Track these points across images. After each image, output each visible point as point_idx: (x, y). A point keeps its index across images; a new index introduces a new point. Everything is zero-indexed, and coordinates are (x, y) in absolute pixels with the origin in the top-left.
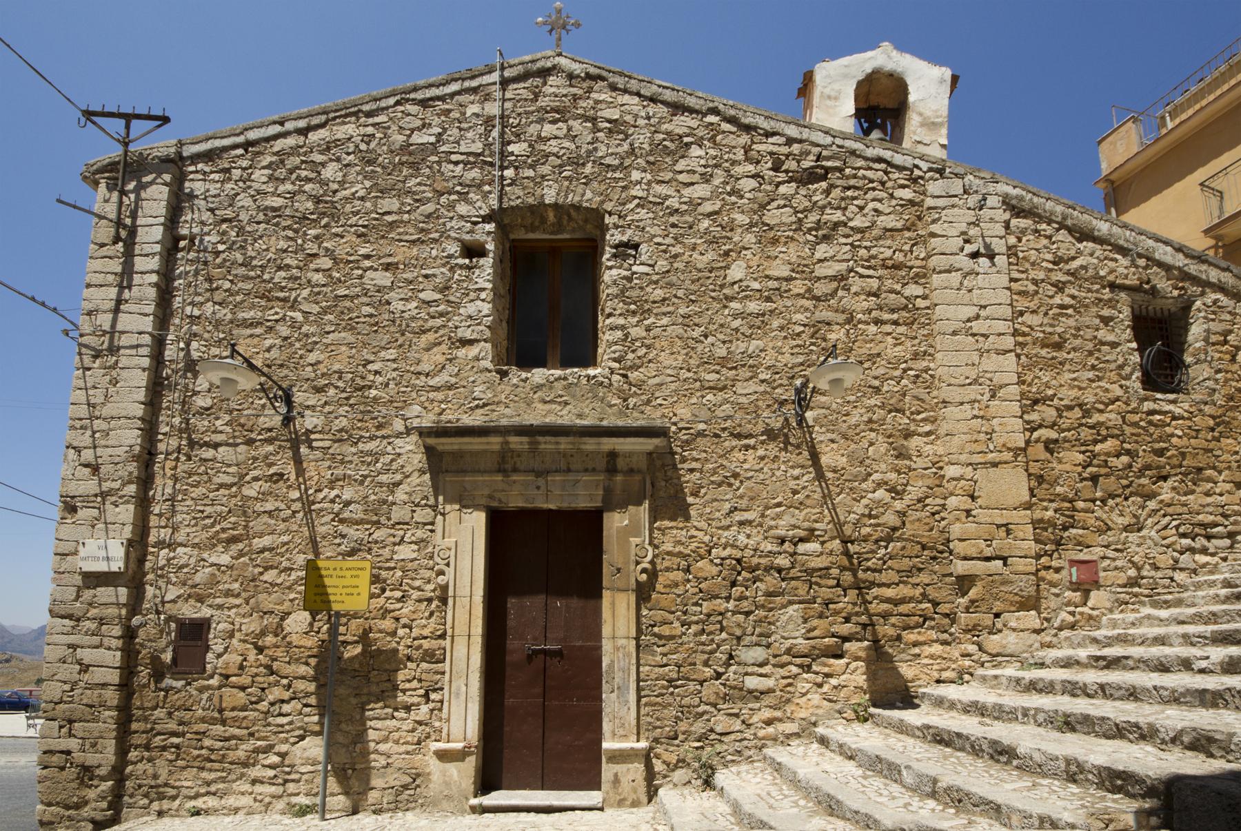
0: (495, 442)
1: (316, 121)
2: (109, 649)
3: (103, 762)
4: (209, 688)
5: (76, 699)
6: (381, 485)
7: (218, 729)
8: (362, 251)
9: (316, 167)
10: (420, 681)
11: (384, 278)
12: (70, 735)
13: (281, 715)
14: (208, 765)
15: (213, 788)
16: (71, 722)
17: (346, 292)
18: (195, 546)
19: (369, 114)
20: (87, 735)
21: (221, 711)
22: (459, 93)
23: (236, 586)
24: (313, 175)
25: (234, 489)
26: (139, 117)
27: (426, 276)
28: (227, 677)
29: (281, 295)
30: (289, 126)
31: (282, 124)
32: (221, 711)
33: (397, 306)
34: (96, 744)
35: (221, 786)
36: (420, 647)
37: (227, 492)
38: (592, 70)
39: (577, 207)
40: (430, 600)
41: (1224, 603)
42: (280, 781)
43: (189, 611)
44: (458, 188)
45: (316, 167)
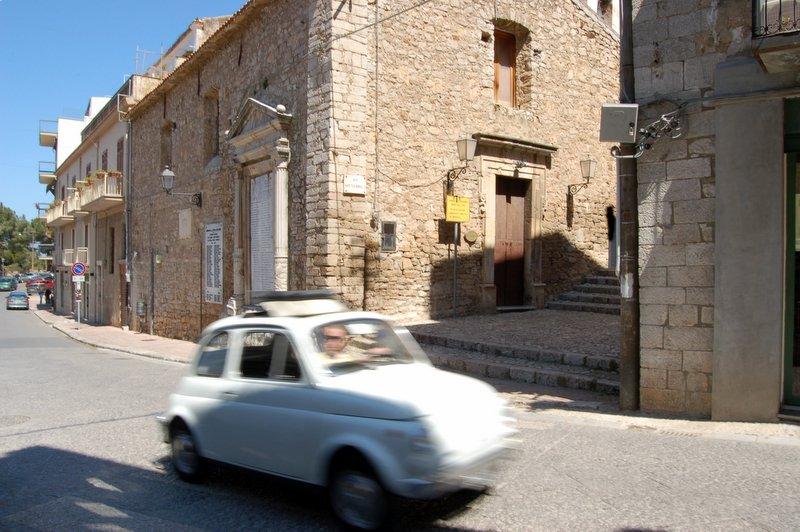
4: (397, 258)
7: (402, 280)
11: (454, 44)
23: (405, 205)
33: (460, 61)
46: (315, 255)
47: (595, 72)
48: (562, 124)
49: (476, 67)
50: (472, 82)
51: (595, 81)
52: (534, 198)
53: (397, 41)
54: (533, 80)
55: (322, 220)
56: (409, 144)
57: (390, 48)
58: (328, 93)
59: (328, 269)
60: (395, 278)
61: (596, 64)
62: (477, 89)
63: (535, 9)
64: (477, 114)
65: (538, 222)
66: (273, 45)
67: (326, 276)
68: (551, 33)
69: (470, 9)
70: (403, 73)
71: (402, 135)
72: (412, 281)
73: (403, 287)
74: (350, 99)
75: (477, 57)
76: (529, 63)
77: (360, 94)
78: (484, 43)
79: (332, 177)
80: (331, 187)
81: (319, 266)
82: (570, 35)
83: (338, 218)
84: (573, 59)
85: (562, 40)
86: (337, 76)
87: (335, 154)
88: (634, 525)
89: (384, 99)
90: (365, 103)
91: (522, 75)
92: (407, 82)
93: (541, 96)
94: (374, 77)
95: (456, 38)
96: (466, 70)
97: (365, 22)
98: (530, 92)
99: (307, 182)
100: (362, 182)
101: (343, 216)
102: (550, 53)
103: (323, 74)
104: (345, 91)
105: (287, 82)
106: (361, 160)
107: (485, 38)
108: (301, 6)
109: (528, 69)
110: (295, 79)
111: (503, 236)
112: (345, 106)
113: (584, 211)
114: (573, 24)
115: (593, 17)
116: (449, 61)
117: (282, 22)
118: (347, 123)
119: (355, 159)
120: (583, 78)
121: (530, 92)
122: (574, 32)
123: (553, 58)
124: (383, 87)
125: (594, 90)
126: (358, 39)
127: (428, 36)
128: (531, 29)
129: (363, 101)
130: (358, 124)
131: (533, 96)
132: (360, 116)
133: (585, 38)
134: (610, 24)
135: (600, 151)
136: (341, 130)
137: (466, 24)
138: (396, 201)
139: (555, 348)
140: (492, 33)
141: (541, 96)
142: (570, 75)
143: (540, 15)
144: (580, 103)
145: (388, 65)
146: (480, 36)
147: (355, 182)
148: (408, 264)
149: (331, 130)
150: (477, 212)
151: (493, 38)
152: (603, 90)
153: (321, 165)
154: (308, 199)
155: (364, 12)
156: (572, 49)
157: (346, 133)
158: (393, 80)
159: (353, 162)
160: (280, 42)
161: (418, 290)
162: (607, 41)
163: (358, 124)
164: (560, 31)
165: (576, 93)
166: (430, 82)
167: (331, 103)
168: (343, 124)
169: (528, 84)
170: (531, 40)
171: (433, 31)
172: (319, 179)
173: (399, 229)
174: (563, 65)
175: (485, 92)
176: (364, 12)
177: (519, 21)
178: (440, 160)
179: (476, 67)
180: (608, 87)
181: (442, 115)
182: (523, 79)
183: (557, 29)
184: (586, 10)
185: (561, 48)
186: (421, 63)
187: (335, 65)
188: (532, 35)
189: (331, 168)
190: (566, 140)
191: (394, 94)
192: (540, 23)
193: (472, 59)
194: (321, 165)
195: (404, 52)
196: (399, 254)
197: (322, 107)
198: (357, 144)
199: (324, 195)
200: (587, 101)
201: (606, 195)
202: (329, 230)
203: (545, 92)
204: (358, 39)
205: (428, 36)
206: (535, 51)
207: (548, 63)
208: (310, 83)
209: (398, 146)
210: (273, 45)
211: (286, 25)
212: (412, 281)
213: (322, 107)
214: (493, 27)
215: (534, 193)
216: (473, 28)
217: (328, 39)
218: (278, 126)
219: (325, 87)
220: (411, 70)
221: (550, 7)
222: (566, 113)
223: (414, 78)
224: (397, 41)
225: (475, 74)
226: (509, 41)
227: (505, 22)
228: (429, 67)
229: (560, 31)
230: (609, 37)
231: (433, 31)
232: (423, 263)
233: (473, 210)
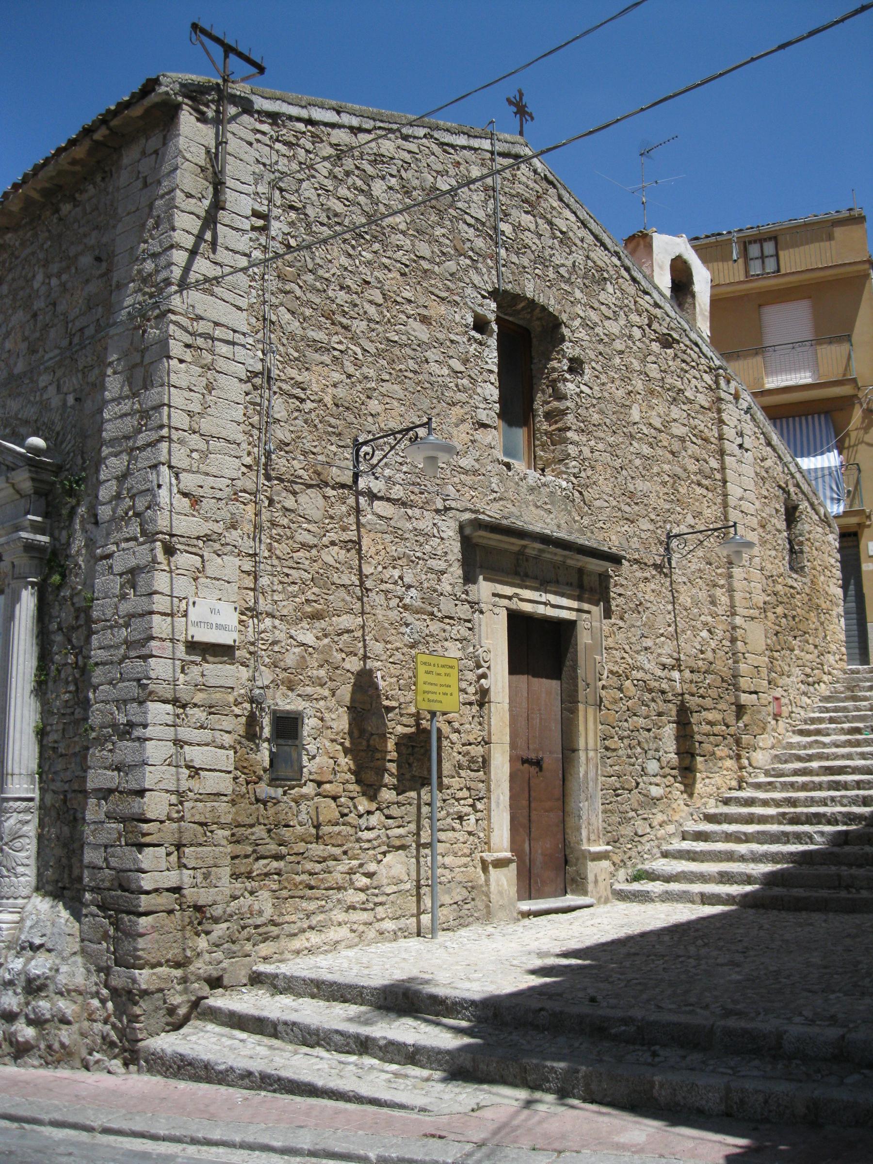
0: (516, 543)
1: (368, 124)
2: (222, 747)
3: (218, 898)
4: (305, 797)
5: (188, 816)
6: (431, 570)
7: (317, 849)
8: (406, 294)
9: (368, 179)
10: (469, 789)
11: (421, 332)
12: (182, 866)
13: (368, 829)
14: (309, 893)
15: (314, 920)
16: (179, 846)
17: (396, 338)
18: (282, 618)
19: (406, 138)
20: (200, 864)
21: (317, 827)
22: (464, 148)
23: (322, 673)
24: (365, 188)
25: (314, 552)
26: (240, 55)
27: (452, 341)
28: (319, 784)
29: (344, 321)
30: (346, 119)
31: (338, 113)
32: (317, 827)
33: (434, 367)
34: (209, 873)
35: (321, 917)
36: (468, 753)
37: (308, 555)
38: (551, 178)
39: (544, 309)
40: (471, 704)
41: (845, 734)
42: (371, 905)
43: (288, 703)
44: (471, 253)
45: (368, 179)
46: (111, 791)
47: (675, 413)
48: (627, 509)
49: (465, 382)
50: (457, 411)
51: (678, 430)
52: (581, 661)
53: (308, 312)
54: (570, 418)
55: (133, 707)
56: (332, 536)
57: (295, 326)
58: (158, 407)
59: (145, 827)
60: (301, 847)
61: (677, 397)
62: (467, 426)
63: (568, 281)
64: (468, 479)
65: (591, 710)
66: (20, 313)
67: (140, 846)
68: (599, 330)
69: (451, 266)
70: (322, 380)
71: (317, 515)
72: (337, 851)
73: (318, 867)
74: (206, 425)
75: (465, 361)
76: (560, 385)
77: (228, 415)
78: (478, 336)
79: (160, 603)
80: (160, 625)
81: (123, 820)
82: (630, 337)
83: (175, 701)
84: (638, 384)
85: (619, 345)
86: (181, 372)
87: (170, 551)
88: (408, 1156)
89: (281, 433)
90: (241, 437)
91: (547, 408)
92: (328, 400)
93: (586, 452)
94: (261, 379)
95: (425, 320)
96: (446, 386)
97: (243, 262)
98: (565, 441)
99: (95, 614)
100: (230, 617)
101: (184, 697)
102: (599, 368)
103: (145, 366)
104: (196, 408)
105: (52, 390)
106: (229, 566)
107: (480, 325)
108: (97, 227)
109: (560, 397)
110: (72, 382)
111: (521, 742)
112: (195, 441)
113: (673, 689)
114: (634, 318)
115: (668, 307)
116: (411, 363)
117: (46, 264)
118: (199, 479)
119: (215, 564)
120: (657, 422)
121: (565, 441)
122: (637, 333)
123: (604, 378)
124: (280, 408)
125: (676, 446)
126: (227, 295)
127: (372, 310)
128: (564, 317)
129: (236, 433)
130: (223, 483)
131: (572, 450)
132: (228, 466)
133: (655, 347)
134: (692, 321)
135: (693, 567)
136: (185, 495)
137: (444, 294)
138: (302, 665)
139: (739, 1014)
140: (492, 317)
141: (586, 452)
142: (635, 414)
143: (578, 294)
144: (655, 469)
145: (288, 361)
146: (470, 320)
147: (215, 617)
148: (329, 810)
149: (163, 493)
150: (471, 690)
151: (495, 327)
152: (692, 449)
153: (133, 575)
154: (98, 655)
155: (242, 243)
156: (636, 365)
157: (195, 501)
158: (298, 394)
159: (209, 572)
160: (39, 304)
161: (351, 872)
162: (695, 356)
163: (223, 483)
164: (614, 327)
165: (646, 450)
166: (374, 405)
167: (165, 432)
168: (189, 481)
169: (559, 425)
170: (563, 339)
171: (380, 300)
172: (125, 608)
173: (310, 724)
174: (621, 393)
175: (480, 435)
176: (242, 243)
177: (542, 300)
178: (396, 573)
179: (465, 382)
180: (699, 442)
181: (399, 477)
182: (548, 416)
183: (607, 323)
184: (655, 295)
185: (617, 361)
186: (358, 364)
187: (176, 349)
188: (566, 331)
189: (161, 581)
190: (635, 543)
191: (300, 422)
192: (579, 309)
193: (458, 366)
194: (133, 575)
195: (320, 336)
196: (309, 789)
197: (142, 439)
198: (219, 528)
199: (140, 646)
200: (666, 467)
201: (709, 655)
202: (149, 732)
203: (592, 443)
204: (227, 295)
205: (372, 310)
206: (571, 360)
207: (596, 388)
208: (114, 385)
209: (310, 539)
210: (20, 313)
211: (55, 268)
212: (337, 851)
213: (142, 439)
214: (494, 306)
215: (581, 648)
216: (457, 304)
217: (161, 291)
218: (27, 486)
219: (152, 396)
220: (336, 376)
221: (594, 281)
222: (631, 487)
223: (341, 392)
224: (308, 312)
225: (462, 397)
226: (526, 343)
227: (516, 298)
228: (372, 373)
229: (614, 327)
230: (696, 349)
231: (380, 300)
232: (361, 809)
233: (464, 685)
